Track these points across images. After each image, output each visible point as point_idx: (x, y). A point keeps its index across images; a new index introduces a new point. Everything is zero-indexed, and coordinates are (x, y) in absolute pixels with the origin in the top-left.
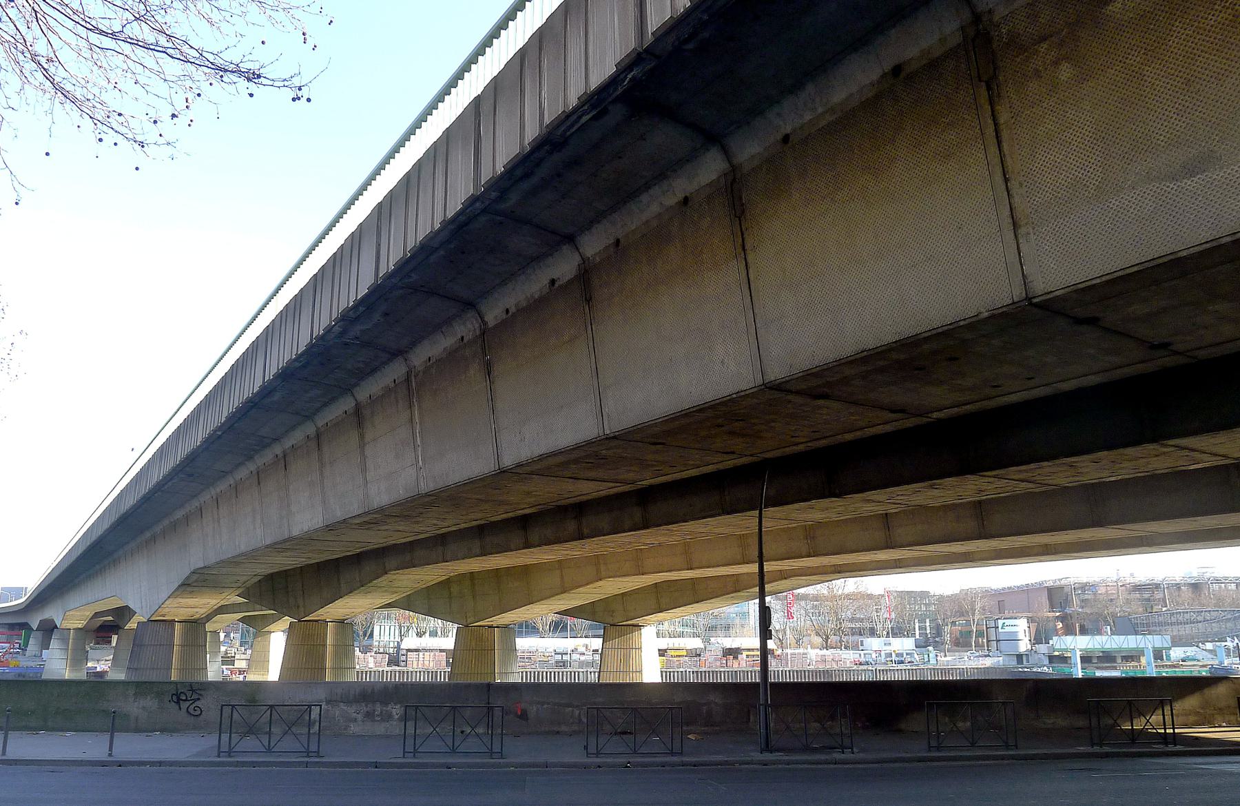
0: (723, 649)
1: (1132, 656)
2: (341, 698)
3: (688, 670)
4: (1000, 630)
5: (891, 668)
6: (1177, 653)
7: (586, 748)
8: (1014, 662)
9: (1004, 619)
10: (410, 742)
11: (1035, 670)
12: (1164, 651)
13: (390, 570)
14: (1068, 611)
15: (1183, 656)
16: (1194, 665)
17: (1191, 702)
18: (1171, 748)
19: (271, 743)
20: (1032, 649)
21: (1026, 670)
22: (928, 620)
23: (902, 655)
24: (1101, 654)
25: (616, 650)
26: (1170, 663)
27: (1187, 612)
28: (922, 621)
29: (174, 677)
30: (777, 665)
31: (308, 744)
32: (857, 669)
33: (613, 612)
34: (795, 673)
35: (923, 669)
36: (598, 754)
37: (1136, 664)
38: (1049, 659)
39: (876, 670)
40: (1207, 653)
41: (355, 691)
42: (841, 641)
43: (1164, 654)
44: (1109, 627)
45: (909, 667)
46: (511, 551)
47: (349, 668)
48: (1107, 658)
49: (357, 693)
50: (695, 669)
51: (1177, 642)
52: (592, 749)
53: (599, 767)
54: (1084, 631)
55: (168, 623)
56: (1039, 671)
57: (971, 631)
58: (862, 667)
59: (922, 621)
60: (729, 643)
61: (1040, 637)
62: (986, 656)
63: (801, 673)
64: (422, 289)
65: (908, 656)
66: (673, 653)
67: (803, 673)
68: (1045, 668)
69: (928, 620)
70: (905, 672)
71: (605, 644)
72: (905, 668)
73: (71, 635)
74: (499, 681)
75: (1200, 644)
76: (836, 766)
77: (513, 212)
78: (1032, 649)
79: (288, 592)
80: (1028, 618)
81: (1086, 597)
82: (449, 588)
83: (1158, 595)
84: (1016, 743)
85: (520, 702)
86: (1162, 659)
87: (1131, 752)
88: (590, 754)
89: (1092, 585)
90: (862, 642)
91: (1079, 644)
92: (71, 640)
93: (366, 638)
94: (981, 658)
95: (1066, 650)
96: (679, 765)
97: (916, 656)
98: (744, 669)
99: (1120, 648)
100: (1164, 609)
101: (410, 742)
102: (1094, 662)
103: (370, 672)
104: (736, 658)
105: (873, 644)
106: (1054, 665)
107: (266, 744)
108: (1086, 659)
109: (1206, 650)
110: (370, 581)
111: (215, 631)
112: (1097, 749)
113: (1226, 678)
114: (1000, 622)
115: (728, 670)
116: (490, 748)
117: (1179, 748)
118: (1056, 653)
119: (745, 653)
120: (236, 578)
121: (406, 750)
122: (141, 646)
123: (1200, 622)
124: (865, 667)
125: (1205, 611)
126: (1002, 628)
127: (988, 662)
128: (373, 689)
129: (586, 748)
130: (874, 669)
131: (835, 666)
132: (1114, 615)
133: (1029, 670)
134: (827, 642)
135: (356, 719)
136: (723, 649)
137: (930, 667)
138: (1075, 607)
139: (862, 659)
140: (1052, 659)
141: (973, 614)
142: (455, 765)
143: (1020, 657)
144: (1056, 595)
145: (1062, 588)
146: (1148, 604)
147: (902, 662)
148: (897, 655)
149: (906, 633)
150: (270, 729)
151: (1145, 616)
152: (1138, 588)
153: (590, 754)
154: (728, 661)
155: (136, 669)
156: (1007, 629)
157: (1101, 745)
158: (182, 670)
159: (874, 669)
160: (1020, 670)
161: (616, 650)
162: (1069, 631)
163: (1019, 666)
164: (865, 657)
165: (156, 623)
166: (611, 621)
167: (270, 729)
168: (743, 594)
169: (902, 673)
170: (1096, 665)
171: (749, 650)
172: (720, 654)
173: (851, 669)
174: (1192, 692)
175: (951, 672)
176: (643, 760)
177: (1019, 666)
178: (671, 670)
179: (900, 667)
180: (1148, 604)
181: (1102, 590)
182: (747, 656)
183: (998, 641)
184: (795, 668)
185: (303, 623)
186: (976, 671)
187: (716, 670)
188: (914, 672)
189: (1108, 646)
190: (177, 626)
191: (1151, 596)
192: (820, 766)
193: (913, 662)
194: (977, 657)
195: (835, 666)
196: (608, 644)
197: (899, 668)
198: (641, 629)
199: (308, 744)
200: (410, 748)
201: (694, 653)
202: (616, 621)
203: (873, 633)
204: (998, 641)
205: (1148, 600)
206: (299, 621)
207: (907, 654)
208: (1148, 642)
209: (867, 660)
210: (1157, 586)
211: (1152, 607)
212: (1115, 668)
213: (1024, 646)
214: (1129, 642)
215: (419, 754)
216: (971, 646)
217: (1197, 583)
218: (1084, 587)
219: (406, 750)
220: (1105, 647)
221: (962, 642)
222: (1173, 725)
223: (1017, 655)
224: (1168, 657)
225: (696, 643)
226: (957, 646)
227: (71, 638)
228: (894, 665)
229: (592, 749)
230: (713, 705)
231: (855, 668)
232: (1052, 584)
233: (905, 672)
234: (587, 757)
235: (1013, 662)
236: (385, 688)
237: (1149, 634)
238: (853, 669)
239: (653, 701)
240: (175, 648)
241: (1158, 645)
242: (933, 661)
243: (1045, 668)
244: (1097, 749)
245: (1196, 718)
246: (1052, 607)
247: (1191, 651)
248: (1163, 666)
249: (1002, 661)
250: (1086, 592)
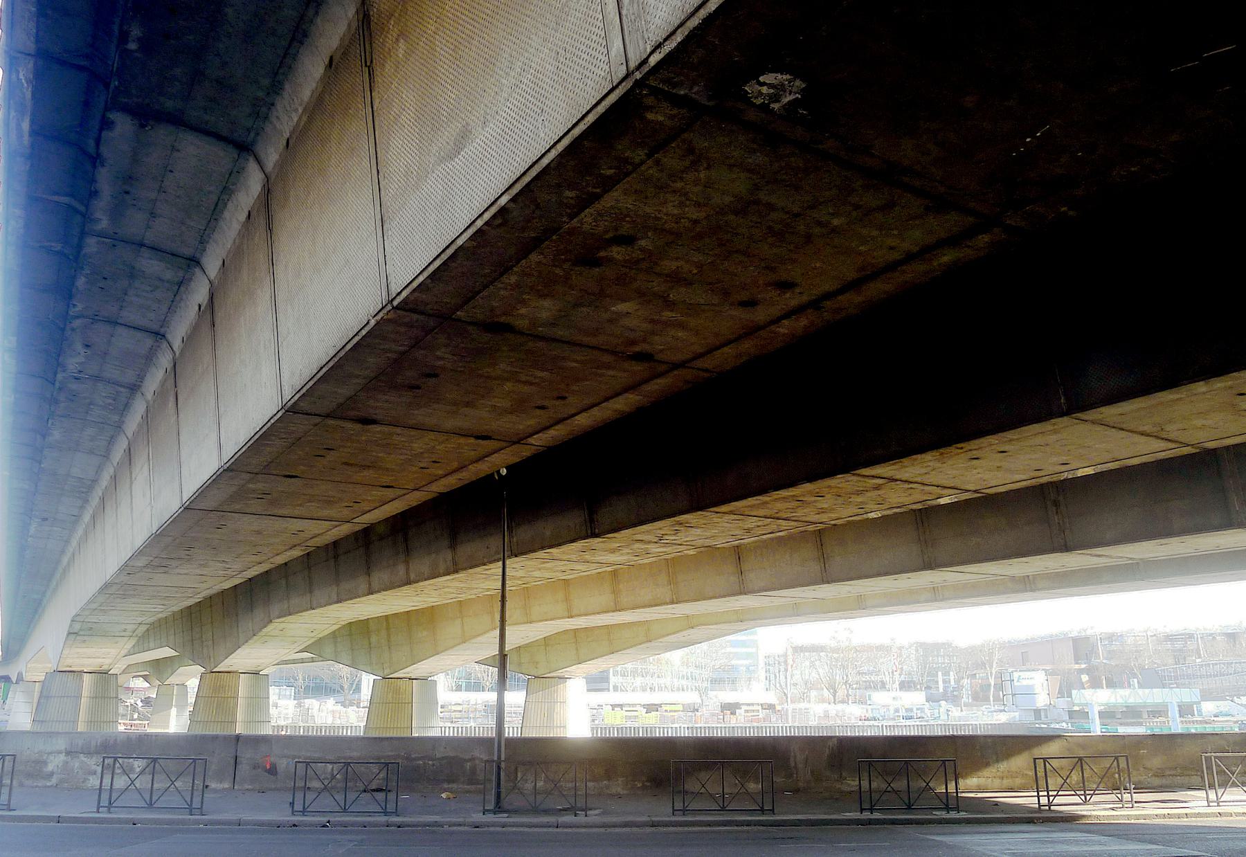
0: (721, 703)
1: (1158, 711)
2: (82, 748)
3: (683, 726)
4: (1016, 683)
5: (898, 724)
6: (1209, 707)
7: (292, 804)
8: (1032, 718)
9: (1020, 671)
10: (105, 796)
11: (1052, 726)
12: (1195, 706)
13: (274, 619)
14: (1095, 662)
15: (1215, 711)
16: (1227, 721)
17: (1020, 762)
18: (953, 815)
19: (153, 798)
20: (1050, 704)
21: (1043, 726)
22: (940, 673)
23: (911, 710)
24: (1124, 709)
25: (546, 704)
26: (1200, 719)
27: (1216, 664)
28: (946, 673)
29: (81, 727)
30: (777, 720)
31: (192, 798)
32: (862, 724)
33: (537, 663)
34: (796, 730)
35: (933, 725)
36: (304, 812)
37: (1164, 719)
38: (1069, 715)
39: (882, 726)
40: (1242, 708)
41: (97, 743)
42: (848, 695)
43: (1195, 709)
44: (1136, 680)
45: (918, 723)
46: (359, 597)
47: (104, 722)
48: (1132, 713)
49: (99, 744)
50: (690, 725)
51: (1207, 696)
52: (298, 807)
53: (294, 825)
54: (1111, 684)
55: (76, 674)
56: (1058, 727)
57: (990, 685)
58: (867, 723)
59: (946, 673)
60: (729, 697)
61: (1065, 690)
62: (1001, 711)
63: (802, 729)
64: (1215, 392)
65: (919, 711)
66: (668, 708)
67: (805, 729)
68: (1064, 724)
69: (940, 673)
70: (914, 728)
71: (528, 697)
72: (914, 723)
73: (36, 688)
74: (417, 735)
75: (1235, 698)
76: (558, 830)
77: (116, 233)
78: (1050, 704)
79: (202, 642)
80: (1046, 671)
81: (1114, 648)
82: (369, 639)
83: (1191, 645)
84: (202, 807)
85: (269, 756)
86: (1193, 715)
87: (928, 819)
88: (296, 811)
89: (1120, 636)
90: (870, 696)
91: (1099, 698)
92: (36, 693)
93: (351, 692)
94: (995, 713)
95: (1086, 705)
96: (383, 826)
97: (926, 711)
98: (741, 725)
99: (1126, 703)
100: (1198, 660)
101: (105, 796)
102: (1117, 717)
103: (351, 727)
104: (733, 713)
105: (879, 697)
106: (1073, 721)
107: (148, 799)
108: (1106, 715)
109: (1242, 705)
110: (261, 630)
111: (183, 684)
112: (866, 815)
113: (1059, 736)
114: (1016, 675)
115: (725, 726)
116: (384, 808)
117: (963, 815)
118: (1076, 708)
119: (744, 708)
120: (124, 627)
121: (675, 808)
122: (48, 697)
123: (1231, 674)
124: (871, 723)
125: (1236, 663)
126: (1018, 681)
127: (1003, 718)
128: (116, 740)
129: (292, 804)
130: (880, 725)
131: (839, 722)
132: (1142, 668)
133: (1046, 726)
134: (834, 696)
135: (96, 772)
136: (721, 703)
137: (940, 722)
138: (1101, 659)
139: (870, 715)
140: (1071, 714)
141: (991, 667)
142: (142, 821)
143: (1037, 712)
144: (1081, 646)
145: (1087, 638)
146: (1180, 657)
147: (911, 718)
148: (907, 710)
149: (919, 687)
150: (947, 790)
151: (1173, 668)
152: (1170, 638)
153: (296, 811)
154: (725, 716)
155: (42, 721)
156: (1025, 683)
157: (871, 810)
158: (90, 722)
159: (880, 725)
160: (1037, 725)
161: (540, 704)
162: (1095, 684)
163: (1036, 722)
164: (872, 712)
165: (64, 673)
166: (534, 672)
167: (947, 790)
168: (657, 644)
169: (910, 729)
170: (1120, 721)
171: (749, 705)
172: (718, 710)
173: (855, 725)
174: (1019, 752)
175: (963, 728)
176: (355, 819)
177: (1036, 722)
178: (665, 726)
179: (908, 723)
180: (1180, 657)
181: (1130, 641)
182: (747, 711)
183: (1013, 695)
184: (796, 724)
185: (214, 674)
186: (989, 727)
187: (713, 725)
188: (924, 728)
189: (1131, 700)
190: (86, 677)
191: (1184, 647)
192: (521, 829)
193: (923, 718)
194: (992, 712)
195: (839, 722)
196: (532, 697)
197: (908, 724)
198: (566, 681)
199: (192, 798)
200: (105, 802)
201: (692, 708)
202: (539, 673)
203: (883, 686)
204: (1013, 695)
205: (1180, 650)
206: (384, 678)
207: (917, 709)
208: (1171, 697)
209: (875, 715)
210: (1191, 636)
211: (1185, 658)
212: (1140, 724)
213: (1042, 700)
214: (1154, 696)
215: (113, 809)
216: (989, 701)
217: (1234, 633)
218: (1111, 637)
219: (675, 808)
220: (1129, 702)
221: (980, 697)
222: (1047, 788)
223: (1034, 710)
224: (1200, 711)
225: (692, 697)
226: (977, 701)
227: (36, 690)
228: (902, 720)
229: (298, 807)
230: (477, 762)
231: (860, 723)
232: (1077, 634)
233: (914, 728)
234: (293, 813)
235: (1030, 718)
236: (128, 738)
237: (1177, 687)
238: (859, 724)
239: (413, 756)
240: (82, 700)
241: (1186, 699)
242: (944, 717)
243: (1064, 724)
244: (866, 815)
245: (1023, 781)
246: (1077, 660)
247: (1224, 706)
248: (1193, 722)
249: (1017, 717)
250: (1114, 643)
